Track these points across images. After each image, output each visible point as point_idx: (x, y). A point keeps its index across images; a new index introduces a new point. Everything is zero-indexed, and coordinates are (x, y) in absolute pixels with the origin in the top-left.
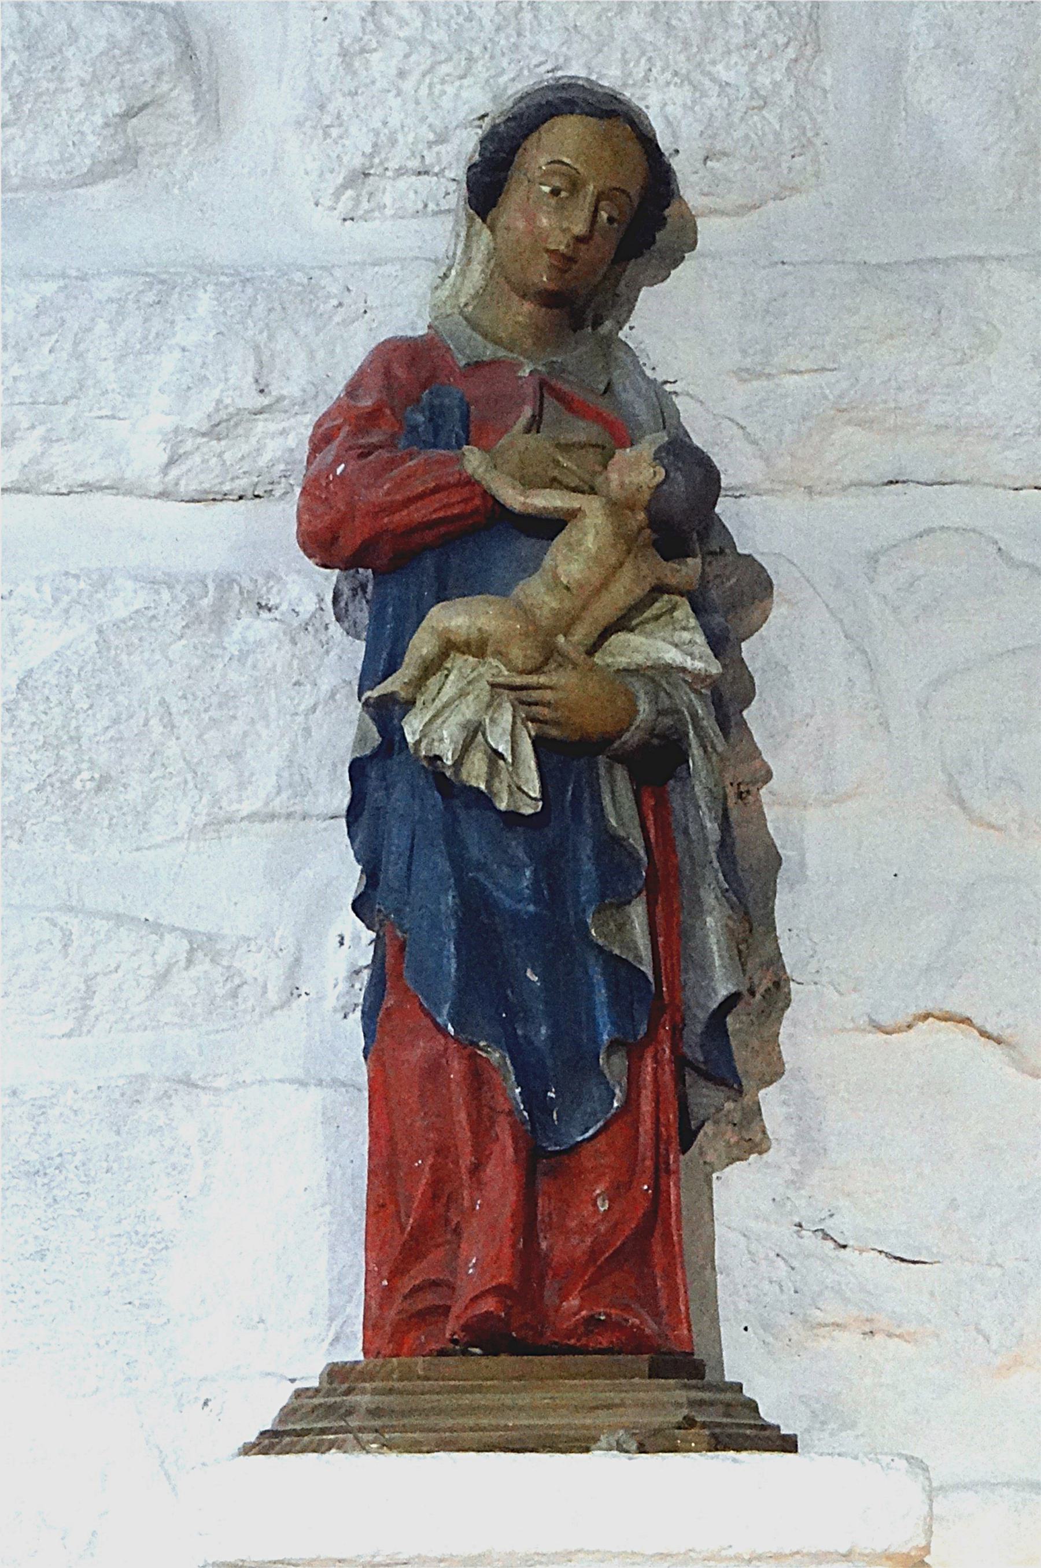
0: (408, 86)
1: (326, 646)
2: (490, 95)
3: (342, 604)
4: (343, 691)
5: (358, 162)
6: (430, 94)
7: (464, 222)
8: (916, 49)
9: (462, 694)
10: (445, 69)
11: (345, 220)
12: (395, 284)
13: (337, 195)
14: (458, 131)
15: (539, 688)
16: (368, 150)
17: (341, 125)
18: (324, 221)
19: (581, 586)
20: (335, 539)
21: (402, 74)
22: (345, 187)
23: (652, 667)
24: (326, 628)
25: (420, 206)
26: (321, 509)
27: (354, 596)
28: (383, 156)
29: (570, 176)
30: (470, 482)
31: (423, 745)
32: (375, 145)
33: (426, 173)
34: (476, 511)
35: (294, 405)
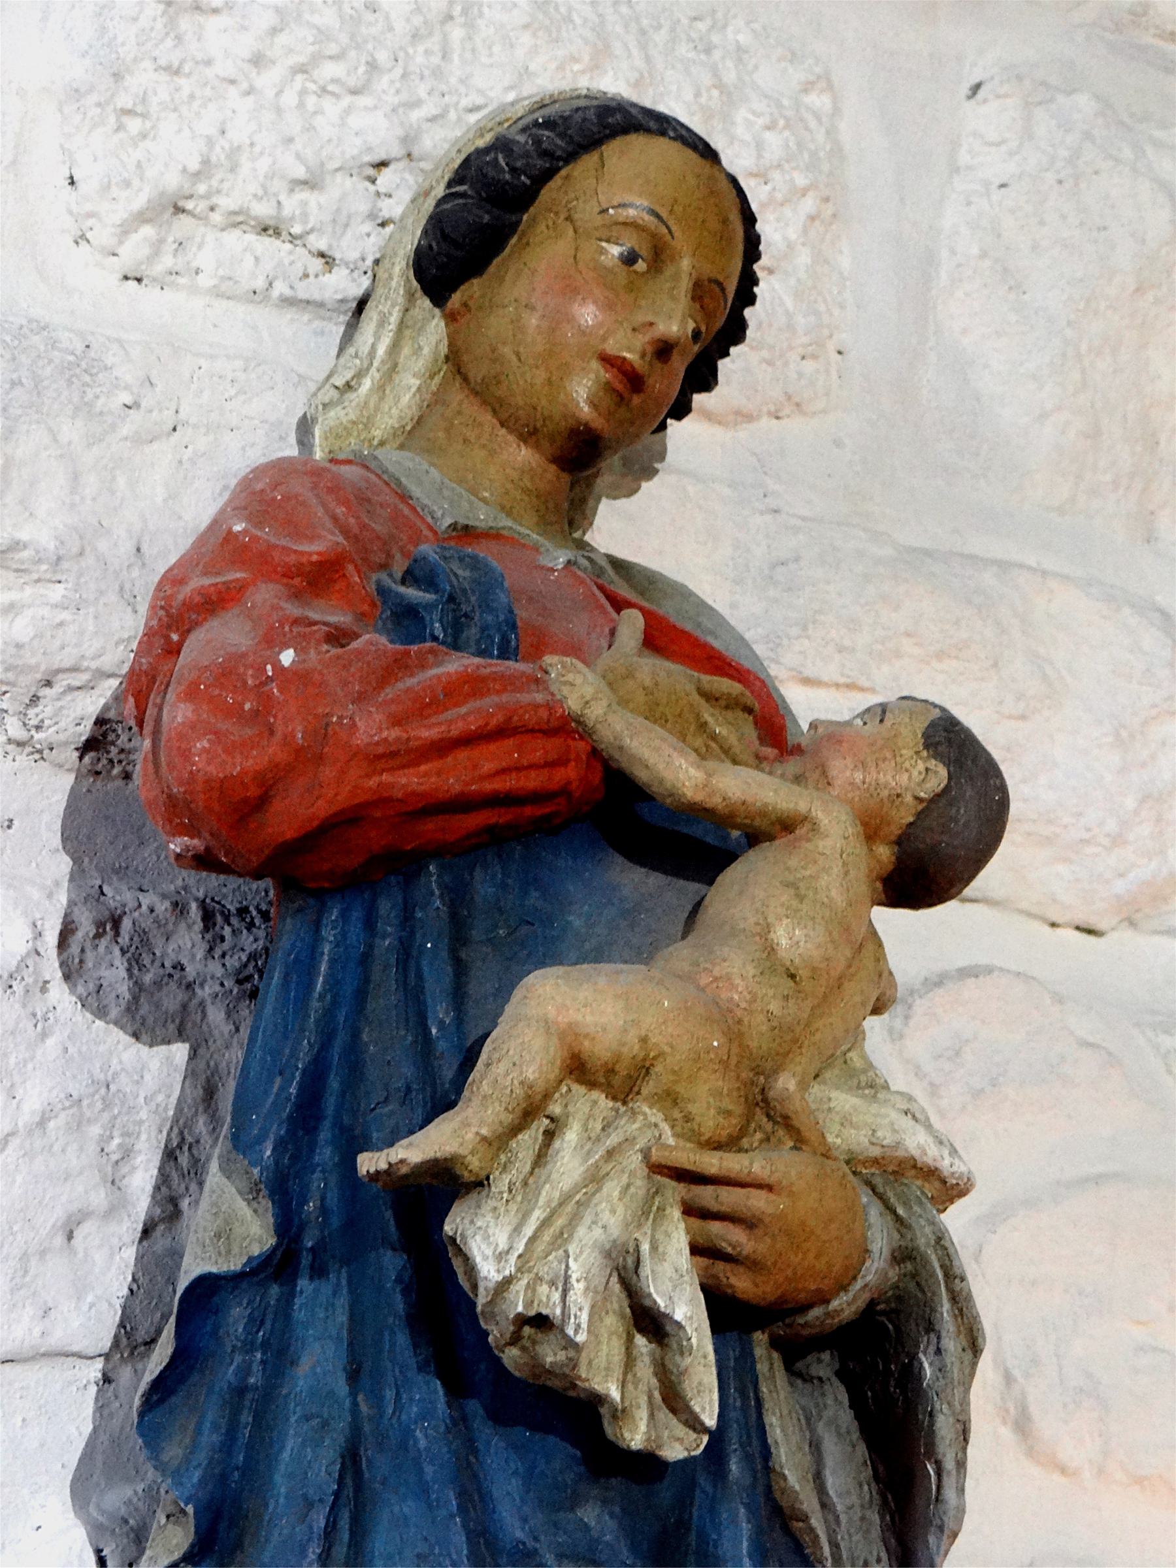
0: (268, 80)
1: (42, 1024)
2: (400, 132)
3: (74, 949)
4: (63, 1117)
5: (172, 181)
6: (301, 105)
7: (400, 300)
8: (953, 252)
9: (595, 1179)
10: (329, 70)
11: (126, 278)
12: (233, 392)
13: (126, 230)
14: (339, 177)
15: (743, 1185)
16: (194, 165)
17: (144, 116)
18: (91, 280)
19: (815, 972)
20: (262, 802)
21: (258, 61)
22: (142, 218)
23: (876, 1161)
24: (44, 989)
25: (260, 284)
26: (240, 732)
27: (98, 936)
28: (214, 183)
29: (654, 236)
30: (566, 728)
31: (519, 1287)
32: (206, 162)
33: (277, 233)
34: (564, 791)
35: (40, 561)
